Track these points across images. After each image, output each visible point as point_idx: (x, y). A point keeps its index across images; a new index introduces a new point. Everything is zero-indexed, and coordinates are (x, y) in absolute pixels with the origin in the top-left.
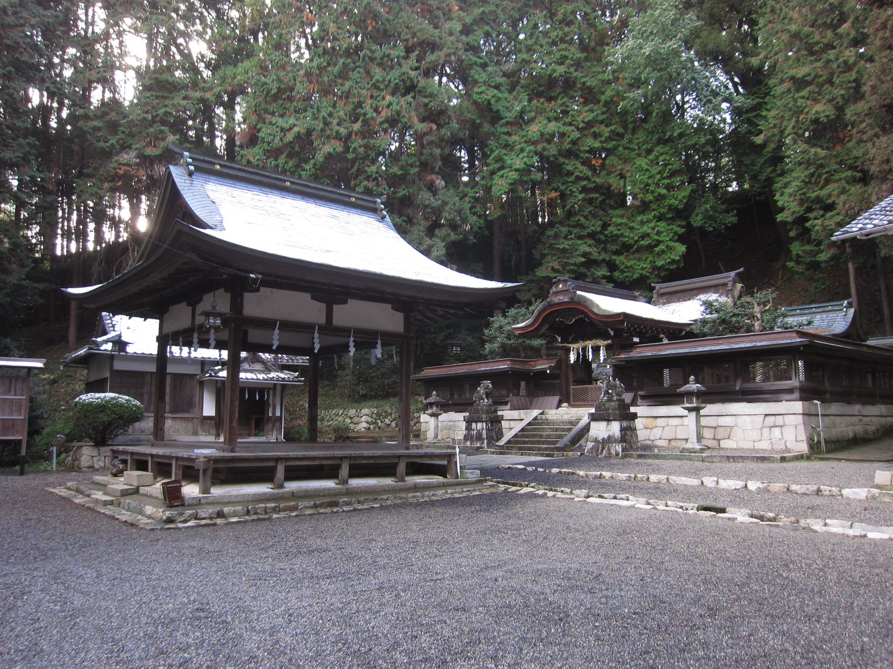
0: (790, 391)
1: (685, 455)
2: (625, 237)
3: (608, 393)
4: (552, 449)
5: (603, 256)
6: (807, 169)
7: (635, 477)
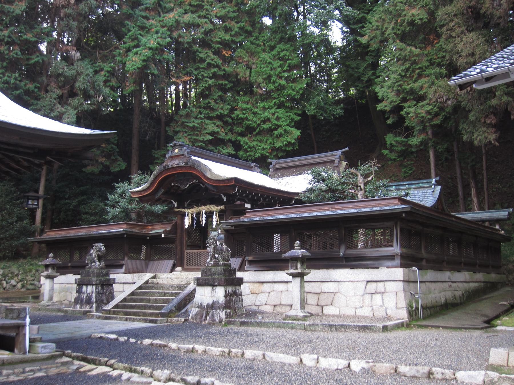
0: (392, 257)
1: (287, 322)
2: (249, 120)
3: (215, 258)
4: (157, 315)
5: (230, 136)
6: (403, 64)
7: (230, 352)
